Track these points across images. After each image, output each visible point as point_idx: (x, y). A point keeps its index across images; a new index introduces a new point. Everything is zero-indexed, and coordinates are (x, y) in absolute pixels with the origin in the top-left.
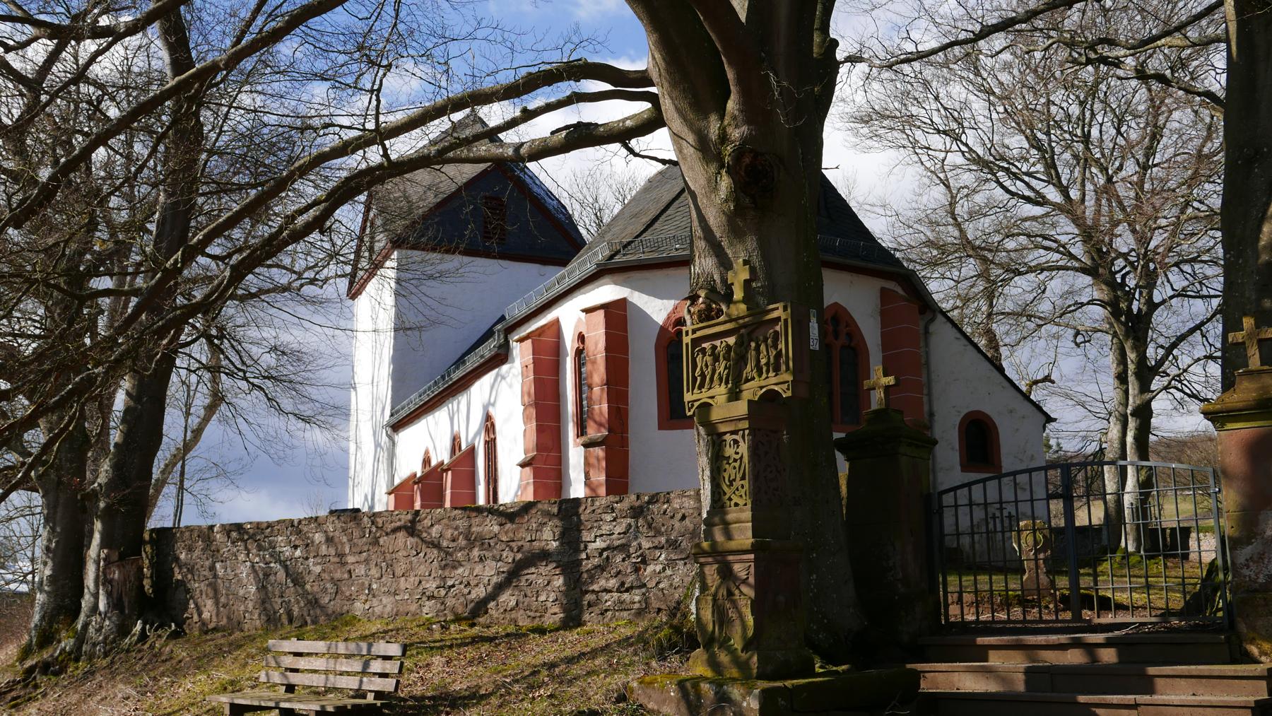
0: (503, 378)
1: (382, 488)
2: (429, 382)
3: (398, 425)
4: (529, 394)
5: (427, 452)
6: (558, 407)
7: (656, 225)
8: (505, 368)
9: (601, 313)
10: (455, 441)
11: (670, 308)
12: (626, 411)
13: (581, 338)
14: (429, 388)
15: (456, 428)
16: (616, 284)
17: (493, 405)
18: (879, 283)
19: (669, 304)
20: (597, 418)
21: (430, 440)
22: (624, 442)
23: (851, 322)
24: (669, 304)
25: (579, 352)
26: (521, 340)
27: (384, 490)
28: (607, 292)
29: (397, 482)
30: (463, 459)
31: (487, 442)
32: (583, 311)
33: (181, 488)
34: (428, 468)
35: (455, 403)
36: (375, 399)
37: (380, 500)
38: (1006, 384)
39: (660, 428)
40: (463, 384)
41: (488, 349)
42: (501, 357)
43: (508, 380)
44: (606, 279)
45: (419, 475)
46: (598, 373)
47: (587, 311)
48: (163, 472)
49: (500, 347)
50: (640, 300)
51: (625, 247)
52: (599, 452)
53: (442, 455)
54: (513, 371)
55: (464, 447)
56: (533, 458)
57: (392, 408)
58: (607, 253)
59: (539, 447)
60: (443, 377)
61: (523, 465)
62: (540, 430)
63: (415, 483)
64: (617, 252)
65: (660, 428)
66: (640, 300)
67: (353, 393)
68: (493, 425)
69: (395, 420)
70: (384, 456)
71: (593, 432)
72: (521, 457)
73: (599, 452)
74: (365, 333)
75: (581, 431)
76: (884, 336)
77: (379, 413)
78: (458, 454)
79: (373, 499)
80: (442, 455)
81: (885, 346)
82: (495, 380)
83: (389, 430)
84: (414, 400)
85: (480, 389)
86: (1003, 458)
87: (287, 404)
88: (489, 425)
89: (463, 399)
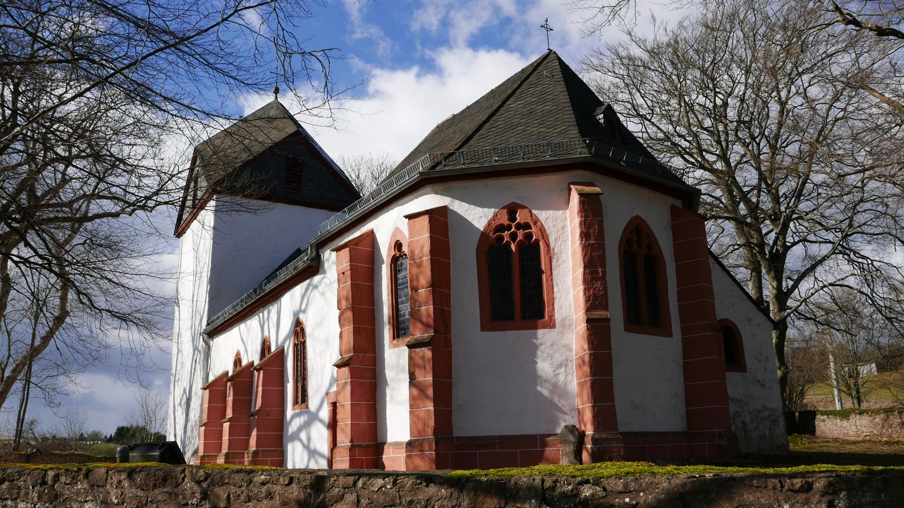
0: (316, 287)
1: (198, 384)
2: (240, 294)
3: (212, 333)
4: (347, 300)
5: (238, 354)
6: (373, 311)
7: (471, 142)
8: (317, 278)
9: (426, 218)
10: (265, 346)
11: (491, 216)
12: (449, 312)
13: (398, 245)
14: (242, 301)
15: (266, 333)
16: (437, 193)
17: (304, 311)
18: (670, 201)
19: (490, 212)
20: (424, 319)
21: (241, 344)
22: (448, 343)
23: (650, 235)
24: (490, 212)
25: (395, 260)
26: (338, 250)
27: (200, 385)
28: (428, 201)
29: (211, 378)
30: (272, 361)
31: (295, 345)
32: (406, 217)
33: (28, 381)
34: (238, 368)
35: (266, 313)
36: (194, 313)
37: (196, 394)
38: (745, 297)
39: (482, 330)
40: (275, 295)
41: (301, 263)
42: (314, 268)
43: (320, 288)
44: (427, 189)
45: (230, 374)
46: (425, 277)
47: (410, 217)
48: (14, 371)
49: (312, 260)
50: (459, 207)
51: (446, 159)
52: (427, 352)
53: (252, 356)
54: (326, 281)
55: (273, 349)
56: (350, 359)
57: (209, 319)
58: (428, 164)
59: (357, 348)
60: (255, 291)
61: (339, 366)
62: (356, 332)
63: (229, 380)
64: (440, 163)
65: (482, 330)
66: (459, 207)
67: (176, 308)
68: (303, 330)
69: (211, 328)
70: (200, 357)
71: (418, 333)
72: (336, 357)
73: (427, 352)
74: (185, 263)
75: (399, 331)
76: (675, 247)
77: (197, 323)
78: (267, 356)
79: (190, 392)
80: (252, 356)
81: (678, 257)
82: (307, 289)
83: (205, 336)
84: (228, 311)
85: (290, 301)
86: (747, 360)
87: (101, 302)
88: (298, 330)
89: (274, 309)
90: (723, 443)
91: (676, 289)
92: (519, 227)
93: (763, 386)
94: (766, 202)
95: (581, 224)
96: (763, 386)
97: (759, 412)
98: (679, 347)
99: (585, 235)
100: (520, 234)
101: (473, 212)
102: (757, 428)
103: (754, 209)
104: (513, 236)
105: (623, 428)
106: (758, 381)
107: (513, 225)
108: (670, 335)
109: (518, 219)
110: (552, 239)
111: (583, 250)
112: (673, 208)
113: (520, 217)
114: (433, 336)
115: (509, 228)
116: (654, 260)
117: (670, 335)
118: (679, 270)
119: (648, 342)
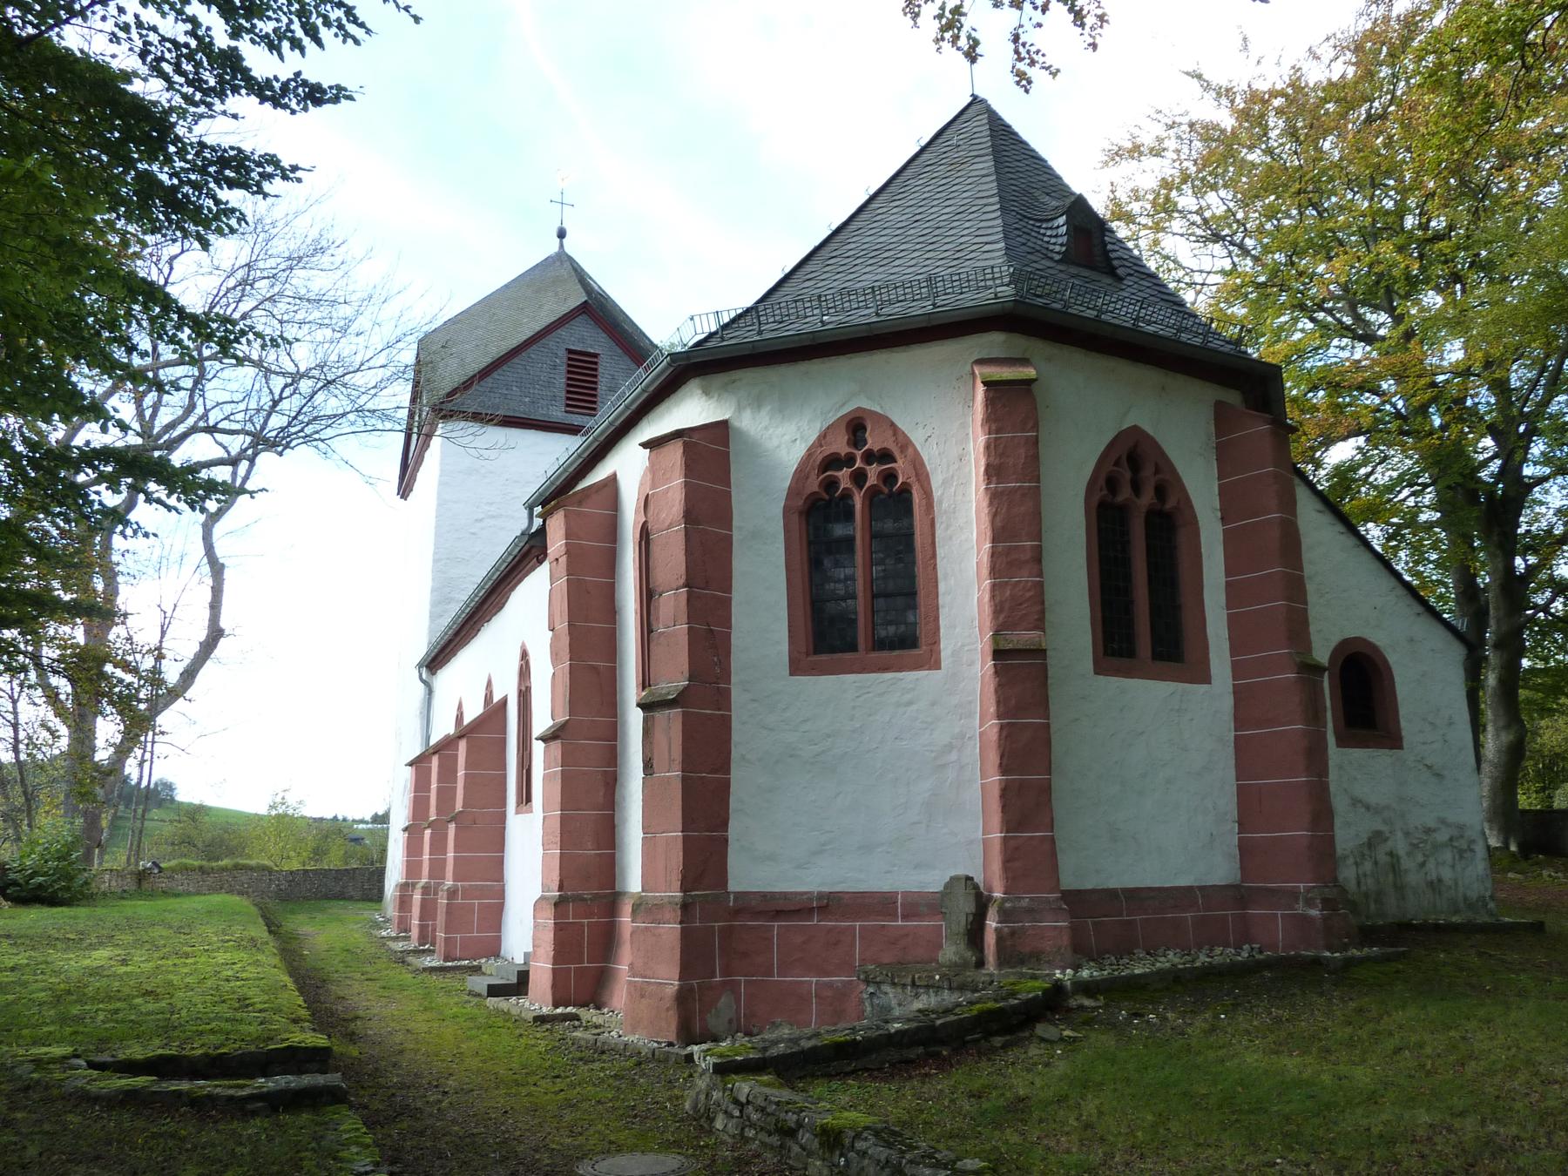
76: (1223, 492)
86: (1403, 723)
90: (1314, 912)
91: (1222, 580)
92: (869, 457)
93: (1439, 775)
94: (1483, 398)
95: (987, 447)
96: (1439, 775)
97: (1428, 831)
98: (1228, 702)
99: (993, 472)
100: (873, 472)
101: (780, 431)
102: (1423, 864)
103: (1458, 410)
104: (859, 478)
105: (1069, 881)
106: (1429, 767)
107: (859, 454)
108: (1205, 678)
109: (870, 441)
110: (936, 482)
111: (991, 504)
112: (1220, 410)
113: (873, 442)
114: (686, 688)
115: (850, 460)
116: (1168, 524)
117: (1205, 678)
118: (1229, 539)
119: (1148, 696)
